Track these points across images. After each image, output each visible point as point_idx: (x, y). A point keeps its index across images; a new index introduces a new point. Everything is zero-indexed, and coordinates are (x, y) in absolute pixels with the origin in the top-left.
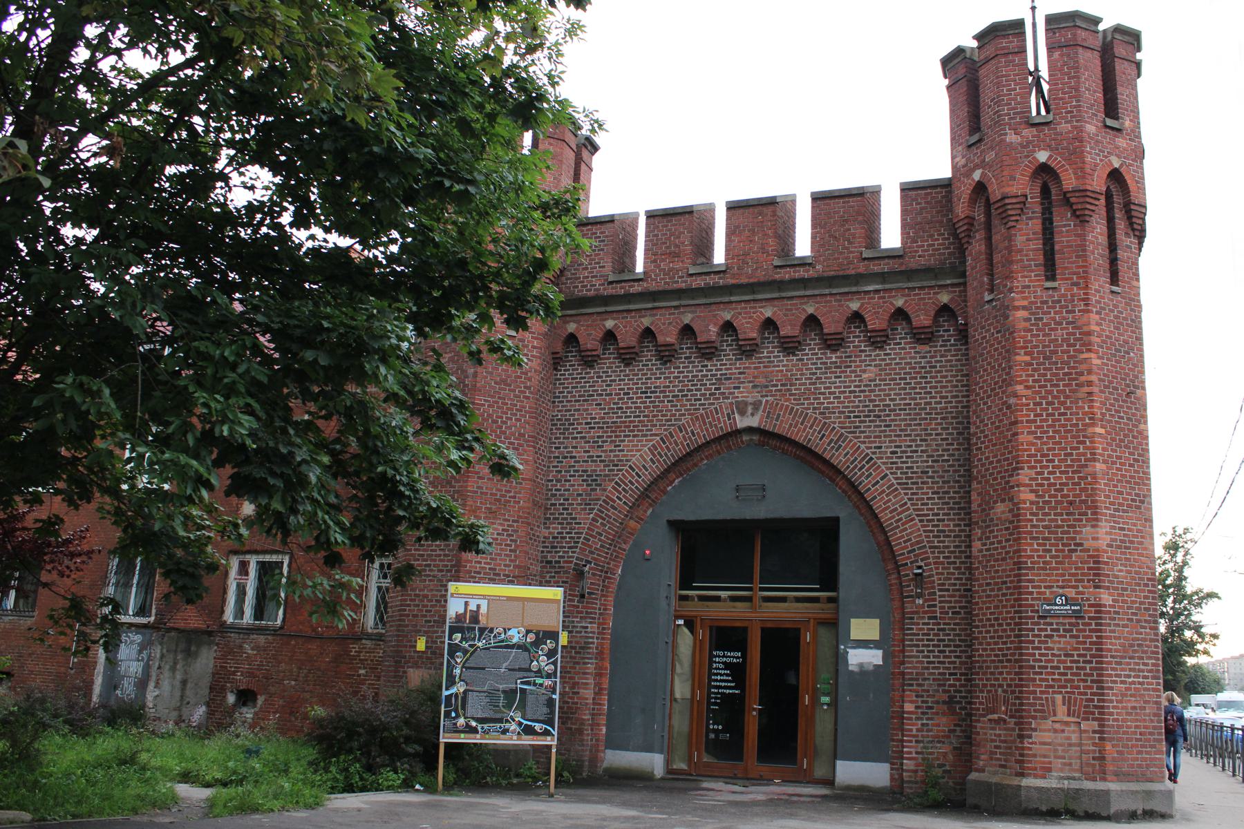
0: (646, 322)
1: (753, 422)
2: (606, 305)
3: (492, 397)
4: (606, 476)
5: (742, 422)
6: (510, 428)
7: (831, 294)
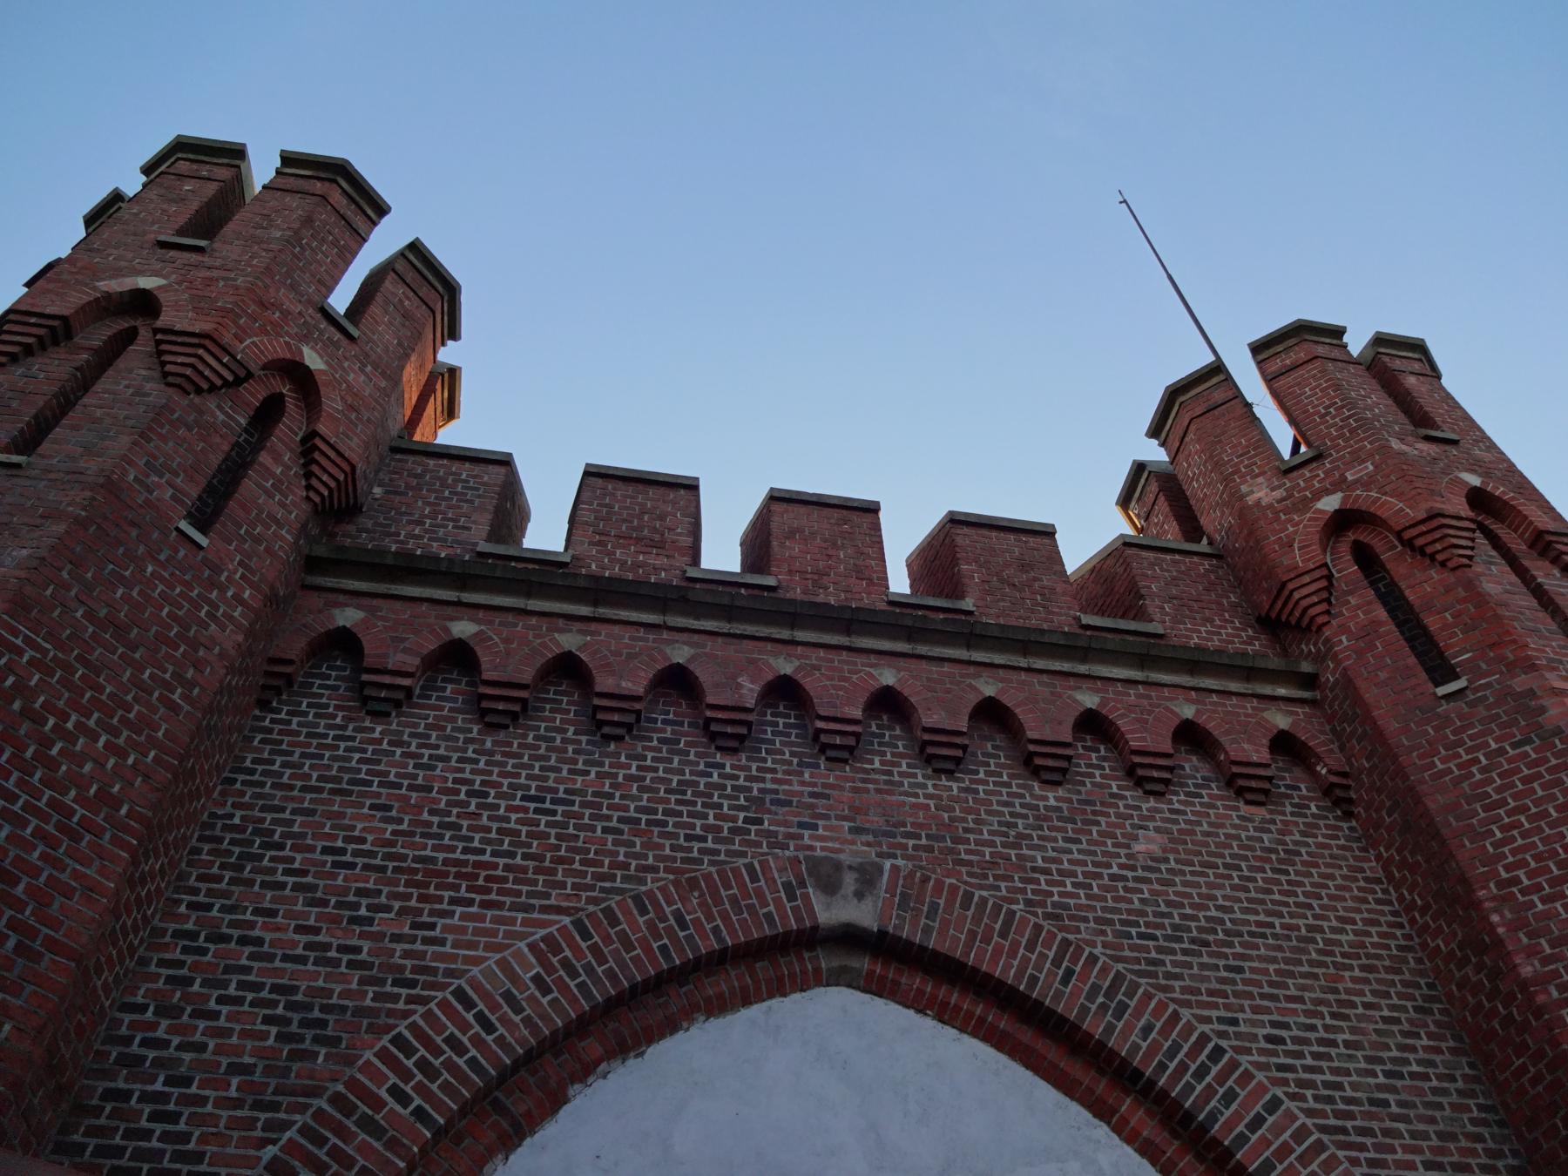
0: (569, 641)
1: (863, 914)
2: (463, 587)
3: (60, 645)
4: (360, 1012)
5: (831, 912)
6: (80, 759)
7: (1029, 670)
